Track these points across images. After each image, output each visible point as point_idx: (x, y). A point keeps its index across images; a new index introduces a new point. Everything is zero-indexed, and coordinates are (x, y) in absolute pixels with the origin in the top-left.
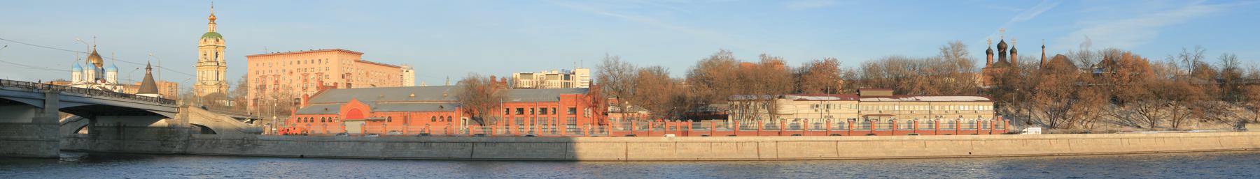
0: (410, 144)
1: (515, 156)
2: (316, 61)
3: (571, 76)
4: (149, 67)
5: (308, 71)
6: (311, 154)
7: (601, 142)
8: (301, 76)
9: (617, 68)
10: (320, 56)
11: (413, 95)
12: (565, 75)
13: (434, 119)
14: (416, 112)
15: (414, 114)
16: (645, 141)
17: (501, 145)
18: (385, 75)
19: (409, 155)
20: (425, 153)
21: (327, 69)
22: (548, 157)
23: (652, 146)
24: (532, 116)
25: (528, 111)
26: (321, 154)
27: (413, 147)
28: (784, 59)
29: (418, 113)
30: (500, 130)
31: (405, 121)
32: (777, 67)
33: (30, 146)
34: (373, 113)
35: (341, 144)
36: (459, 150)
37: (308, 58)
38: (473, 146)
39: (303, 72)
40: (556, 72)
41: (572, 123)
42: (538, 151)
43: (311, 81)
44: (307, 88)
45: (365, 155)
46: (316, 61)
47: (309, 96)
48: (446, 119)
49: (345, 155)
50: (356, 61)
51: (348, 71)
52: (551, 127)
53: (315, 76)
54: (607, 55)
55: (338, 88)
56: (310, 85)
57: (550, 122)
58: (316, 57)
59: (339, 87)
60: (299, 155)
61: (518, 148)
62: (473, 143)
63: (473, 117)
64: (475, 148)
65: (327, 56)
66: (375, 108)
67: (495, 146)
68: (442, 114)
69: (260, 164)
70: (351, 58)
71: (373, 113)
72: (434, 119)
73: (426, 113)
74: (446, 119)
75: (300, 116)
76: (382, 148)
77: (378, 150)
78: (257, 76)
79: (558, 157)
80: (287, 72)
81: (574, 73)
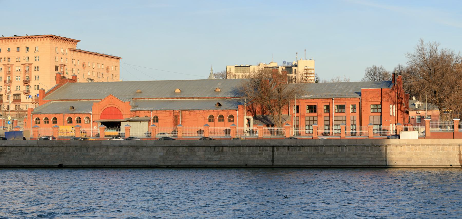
0: (197, 149)
1: (325, 163)
2: (23, 49)
3: (294, 68)
6: (73, 163)
7: (428, 145)
8: (3, 67)
10: (28, 43)
11: (178, 90)
13: (211, 119)
14: (189, 111)
15: (187, 113)
17: (306, 149)
18: (103, 66)
19: (196, 162)
20: (216, 159)
21: (37, 59)
22: (366, 163)
24: (328, 115)
25: (321, 109)
26: (85, 163)
27: (200, 152)
29: (192, 112)
30: (289, 132)
31: (176, 123)
34: (135, 111)
35: (110, 150)
37: (13, 45)
38: (273, 151)
39: (6, 63)
41: (376, 122)
42: (352, 156)
43: (15, 74)
44: (10, 82)
45: (141, 163)
46: (23, 49)
47: (46, 91)
48: (226, 118)
49: (116, 163)
50: (71, 50)
51: (62, 62)
52: (350, 128)
53: (21, 67)
54: (422, 41)
55: (78, 81)
56: (14, 78)
57: (349, 122)
58: (23, 44)
59: (79, 80)
60: (57, 164)
61: (327, 153)
62: (273, 146)
63: (255, 115)
64: (276, 153)
65: (37, 42)
66: (135, 106)
67: (300, 150)
68: (221, 113)
69: (110, 175)
70: (66, 46)
72: (211, 119)
73: (201, 112)
74: (226, 118)
75: (39, 116)
76: (162, 154)
77: (157, 157)
79: (376, 164)
81: (296, 66)
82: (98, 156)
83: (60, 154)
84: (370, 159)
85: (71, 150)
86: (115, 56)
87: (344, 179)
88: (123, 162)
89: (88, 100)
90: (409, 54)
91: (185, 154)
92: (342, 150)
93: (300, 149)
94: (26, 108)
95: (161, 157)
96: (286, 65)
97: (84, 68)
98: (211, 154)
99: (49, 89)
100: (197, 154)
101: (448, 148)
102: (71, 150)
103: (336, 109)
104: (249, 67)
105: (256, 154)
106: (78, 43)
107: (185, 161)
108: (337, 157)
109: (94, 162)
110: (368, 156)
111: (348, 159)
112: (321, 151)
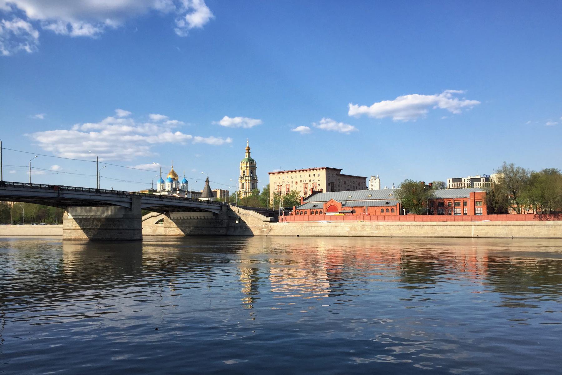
2: (317, 175)
4: (207, 181)
5: (307, 182)
9: (513, 172)
12: (486, 179)
16: (534, 224)
23: (540, 228)
28: (403, 182)
32: (24, 13)
33: (121, 233)
36: (398, 231)
39: (304, 183)
40: (479, 177)
46: (317, 175)
54: (505, 163)
61: (438, 229)
71: (29, 256)
77: (12, 271)
78: (276, 185)
80: (294, 182)
82: (316, 231)
83: (299, 230)
84: (463, 233)
85: (304, 228)
86: (64, 186)
87: (196, 315)
88: (328, 234)
89: (33, 324)
90: (497, 170)
91: (360, 230)
92: (447, 228)
93: (422, 227)
94: (162, 221)
95: (347, 231)
96: (485, 177)
97: (345, 184)
98: (270, 227)
99: (106, 207)
100: (366, 230)
101: (512, 227)
102: (304, 228)
103: (23, 185)
104: (461, 179)
105: (397, 230)
106: (209, 180)
107: (469, 339)
108: (443, 231)
109: (314, 234)
110: (461, 231)
111: (449, 233)
112: (434, 228)
